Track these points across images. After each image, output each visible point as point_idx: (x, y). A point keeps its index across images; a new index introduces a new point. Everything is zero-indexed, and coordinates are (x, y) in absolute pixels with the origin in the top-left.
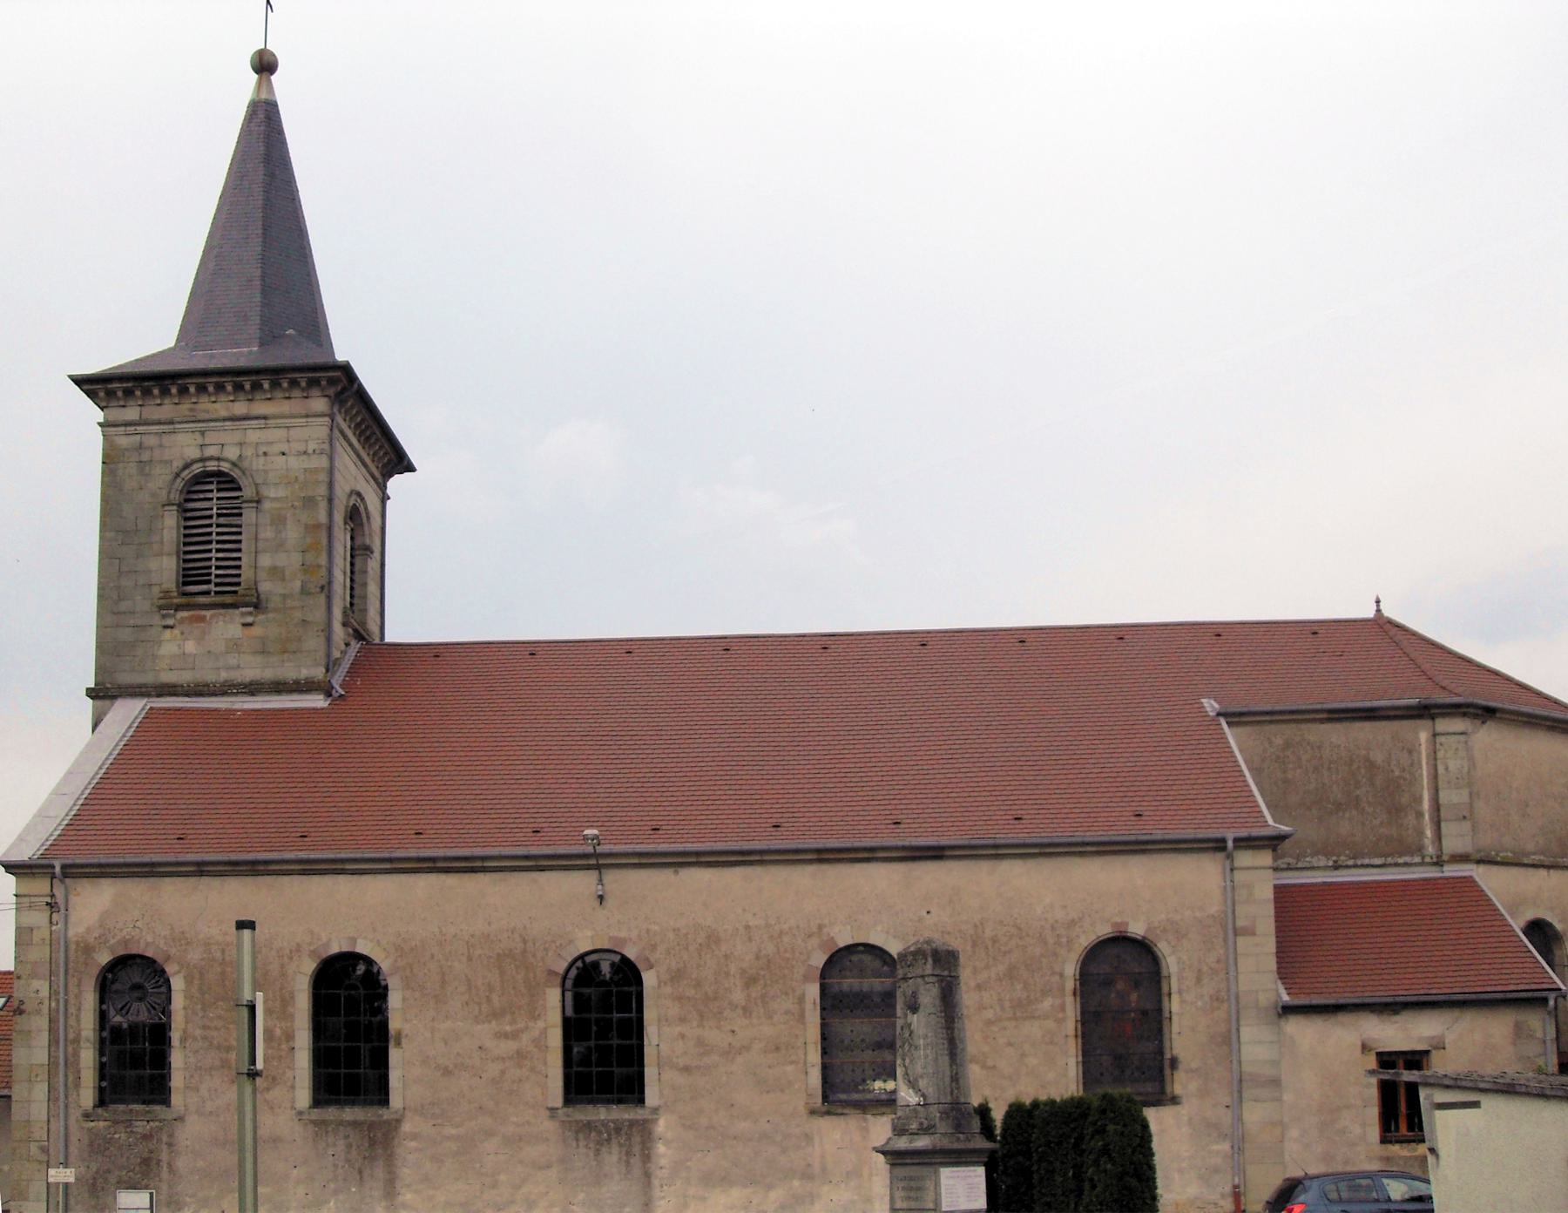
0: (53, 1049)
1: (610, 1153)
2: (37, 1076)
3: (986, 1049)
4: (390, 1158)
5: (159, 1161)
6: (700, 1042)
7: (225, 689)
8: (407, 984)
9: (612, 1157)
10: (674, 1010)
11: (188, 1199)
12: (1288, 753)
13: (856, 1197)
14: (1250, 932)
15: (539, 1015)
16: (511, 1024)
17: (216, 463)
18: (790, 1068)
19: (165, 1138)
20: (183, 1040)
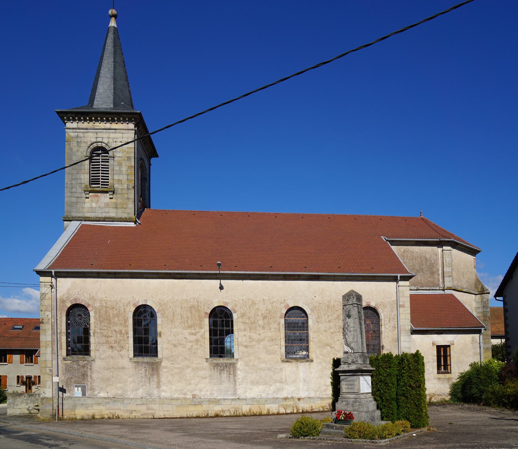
0: (53, 336)
1: (224, 374)
2: (48, 345)
3: (331, 341)
4: (158, 375)
5: (87, 375)
6: (250, 337)
7: (105, 219)
8: (163, 315)
9: (225, 375)
10: (242, 327)
11: (97, 388)
12: (405, 254)
13: (295, 389)
14: (403, 306)
15: (202, 327)
16: (194, 330)
17: (101, 144)
18: (276, 347)
19: (89, 367)
20: (94, 333)
